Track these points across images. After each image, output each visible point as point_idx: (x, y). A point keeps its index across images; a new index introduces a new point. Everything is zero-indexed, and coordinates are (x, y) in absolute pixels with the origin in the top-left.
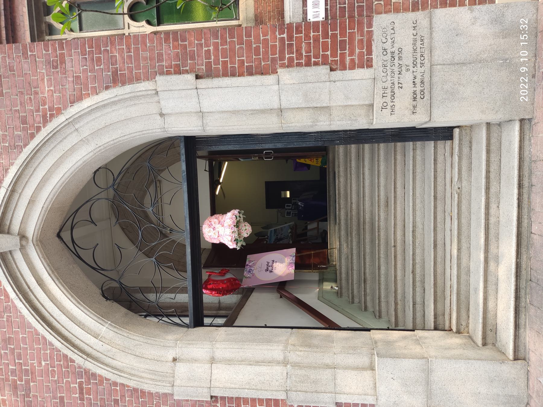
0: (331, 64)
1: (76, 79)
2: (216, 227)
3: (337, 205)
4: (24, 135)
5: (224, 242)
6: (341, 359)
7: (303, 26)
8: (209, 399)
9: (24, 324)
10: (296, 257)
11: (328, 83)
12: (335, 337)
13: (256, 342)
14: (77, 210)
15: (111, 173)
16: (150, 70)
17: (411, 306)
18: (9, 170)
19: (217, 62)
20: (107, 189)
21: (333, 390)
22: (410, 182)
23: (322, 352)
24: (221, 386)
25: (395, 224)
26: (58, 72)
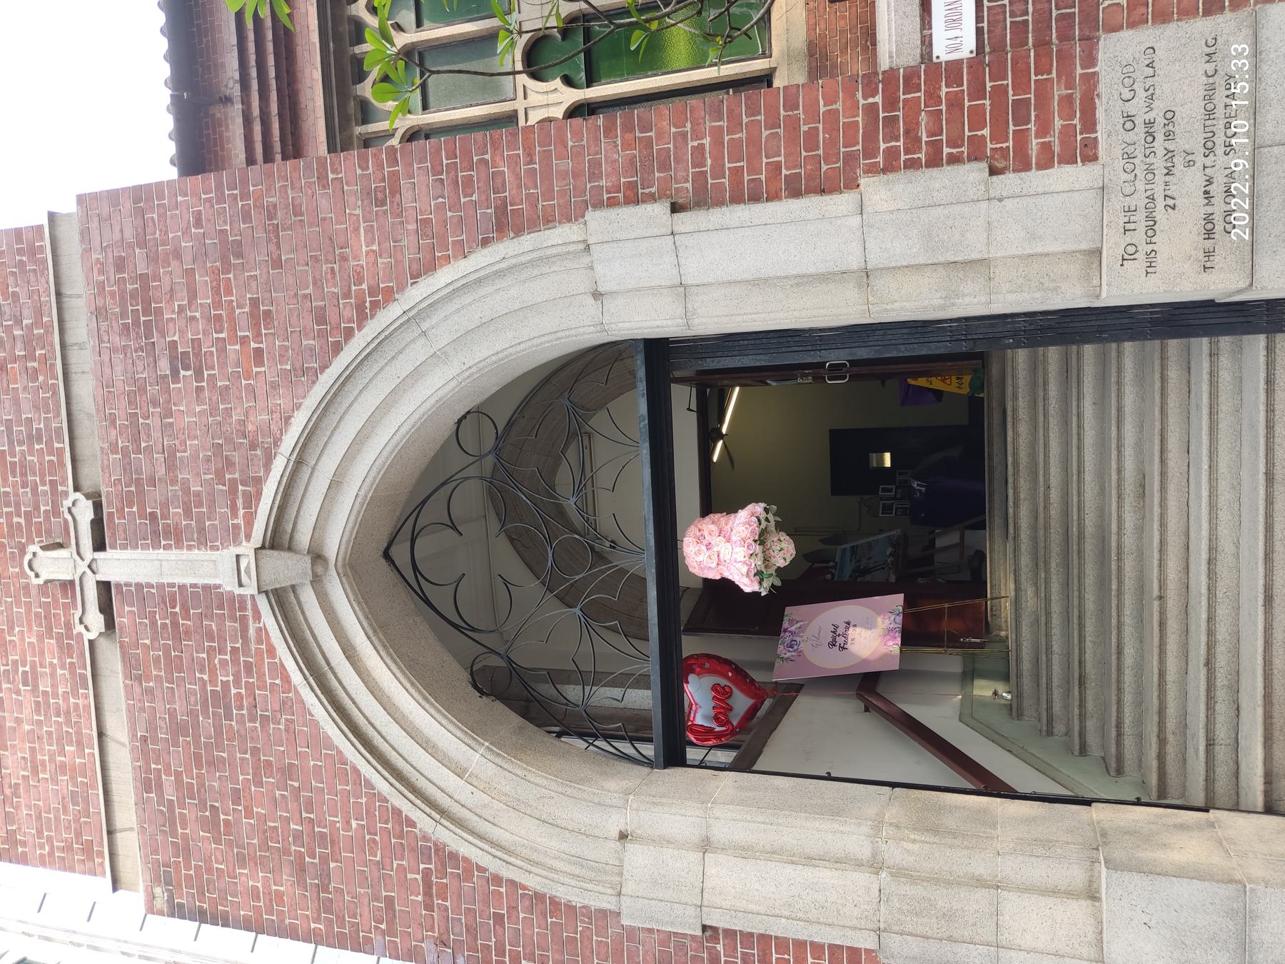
0: (992, 157)
1: (423, 227)
2: (713, 543)
3: (1011, 492)
4: (321, 348)
5: (730, 577)
6: (1012, 867)
7: (922, 73)
8: (699, 933)
9: (318, 740)
10: (905, 616)
11: (984, 205)
12: (999, 814)
13: (806, 812)
14: (424, 502)
15: (491, 422)
16: (573, 200)
17: (1202, 748)
18: (293, 419)
19: (718, 172)
20: (481, 457)
21: (992, 939)
22: (1201, 437)
23: (967, 848)
24: (725, 904)
25: (1163, 543)
26: (385, 212)
